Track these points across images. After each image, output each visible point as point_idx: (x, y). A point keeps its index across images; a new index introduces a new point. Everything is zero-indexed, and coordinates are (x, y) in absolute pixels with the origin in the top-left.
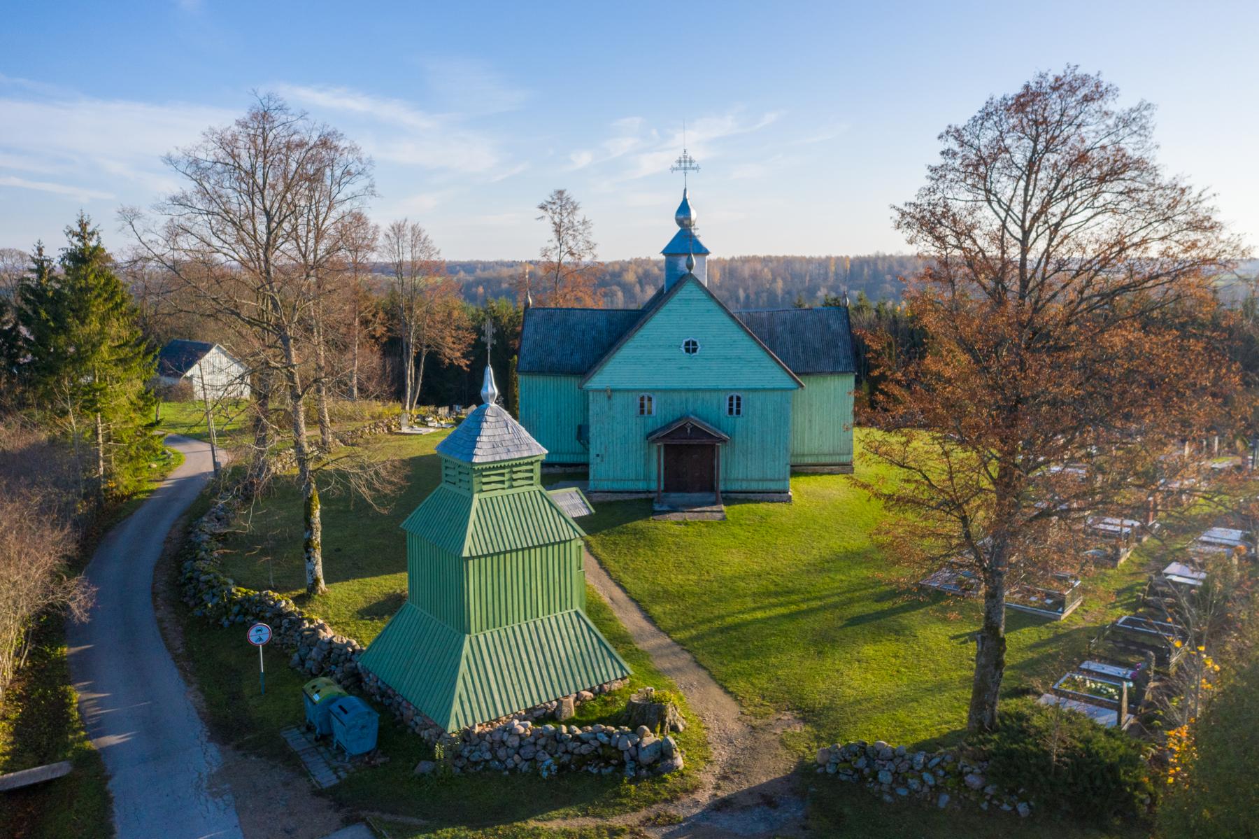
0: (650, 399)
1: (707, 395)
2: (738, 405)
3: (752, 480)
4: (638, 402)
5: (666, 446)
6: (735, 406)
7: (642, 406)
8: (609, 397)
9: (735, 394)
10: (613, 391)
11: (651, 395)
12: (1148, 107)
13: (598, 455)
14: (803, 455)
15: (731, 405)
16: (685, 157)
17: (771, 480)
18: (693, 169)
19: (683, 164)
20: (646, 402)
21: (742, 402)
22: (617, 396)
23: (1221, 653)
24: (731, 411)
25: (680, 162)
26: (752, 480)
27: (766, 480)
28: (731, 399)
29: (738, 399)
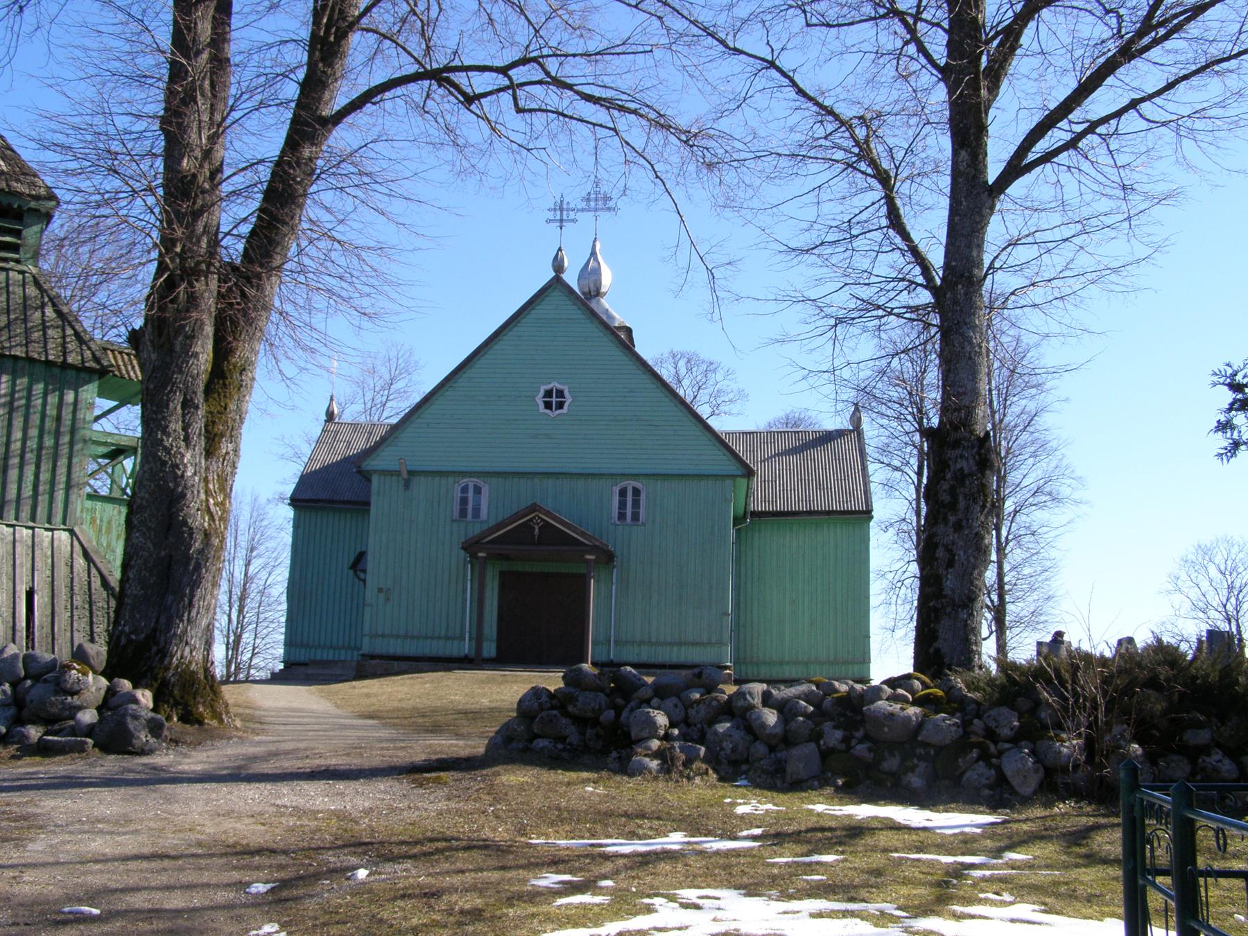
0: (478, 490)
1: (581, 483)
2: (636, 503)
3: (658, 643)
4: (458, 494)
5: (503, 575)
6: (630, 503)
7: (464, 501)
8: (407, 485)
9: (630, 484)
10: (411, 473)
11: (638, 485)
12: (607, 557)
13: (380, 590)
14: (781, 663)
15: (622, 505)
16: (596, 193)
17: (694, 644)
18: (609, 209)
19: (592, 204)
20: (471, 494)
21: (643, 498)
22: (420, 485)
23: (1066, 709)
24: (622, 516)
25: (588, 200)
26: (658, 643)
27: (685, 644)
28: (623, 493)
29: (636, 492)
